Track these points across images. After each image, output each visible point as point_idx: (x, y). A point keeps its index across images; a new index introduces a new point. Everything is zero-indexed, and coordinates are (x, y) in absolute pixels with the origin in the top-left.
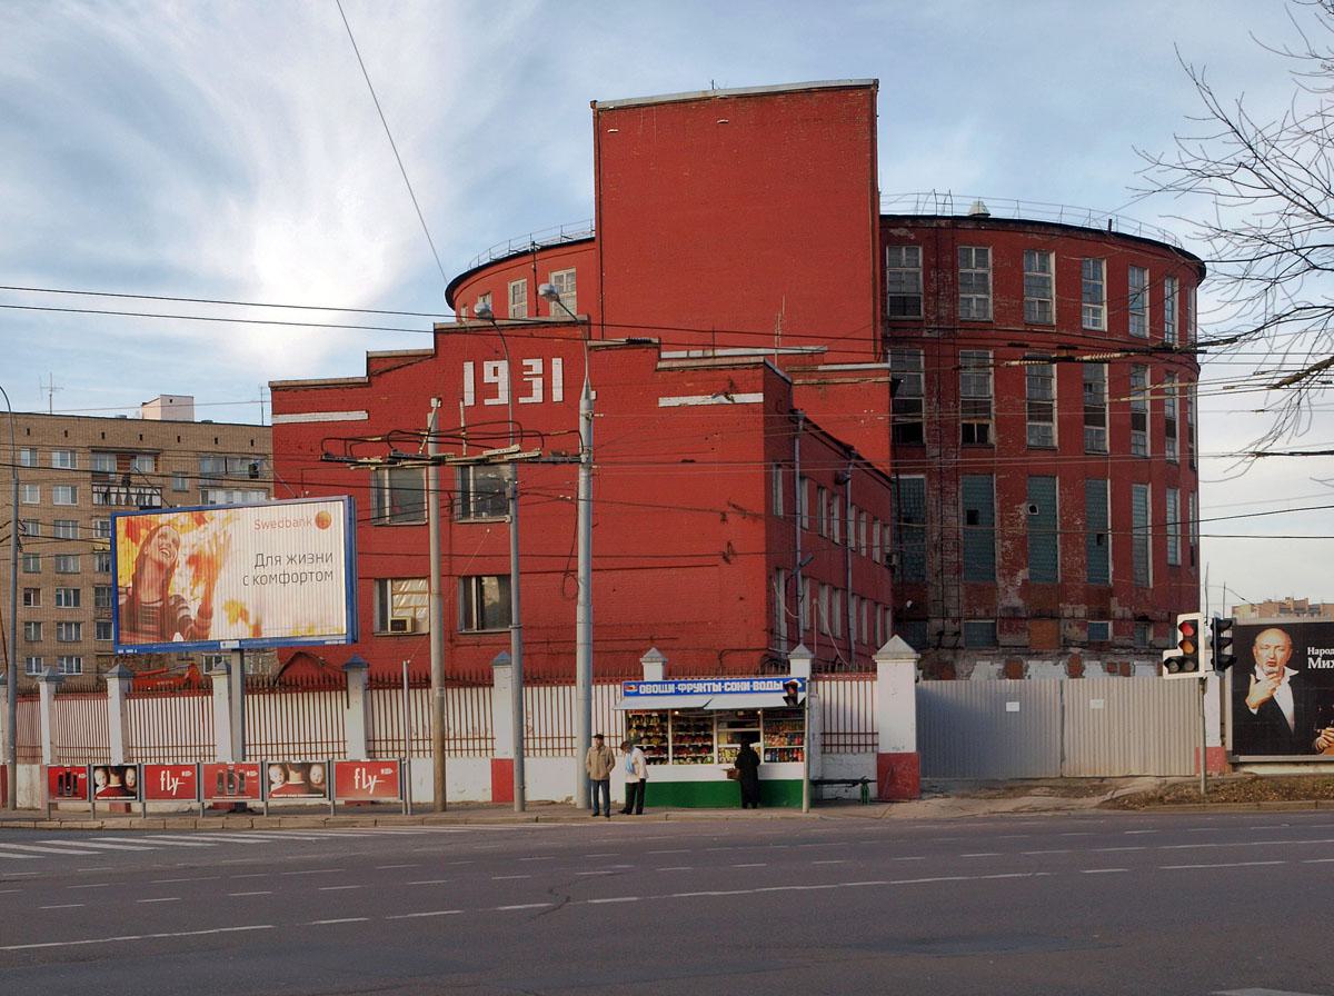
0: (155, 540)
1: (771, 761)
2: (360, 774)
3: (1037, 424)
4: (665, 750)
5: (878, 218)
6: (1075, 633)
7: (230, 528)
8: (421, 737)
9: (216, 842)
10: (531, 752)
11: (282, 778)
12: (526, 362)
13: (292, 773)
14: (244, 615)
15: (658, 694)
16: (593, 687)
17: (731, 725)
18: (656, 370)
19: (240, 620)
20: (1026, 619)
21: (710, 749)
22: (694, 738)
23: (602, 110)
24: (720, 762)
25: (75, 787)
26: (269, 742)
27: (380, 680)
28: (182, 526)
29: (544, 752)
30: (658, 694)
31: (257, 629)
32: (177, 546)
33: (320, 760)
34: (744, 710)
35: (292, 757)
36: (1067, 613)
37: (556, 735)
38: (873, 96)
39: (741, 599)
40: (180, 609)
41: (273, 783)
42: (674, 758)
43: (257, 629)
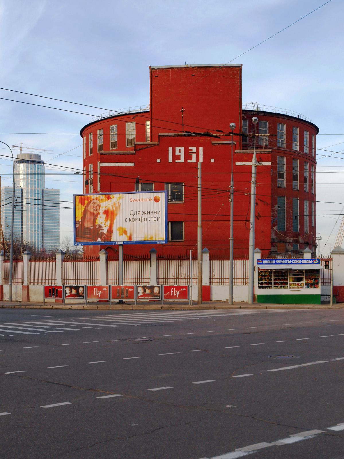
0: (91, 204)
1: (307, 288)
2: (173, 290)
3: (280, 179)
4: (271, 283)
5: (241, 111)
6: (290, 247)
7: (121, 201)
8: (175, 277)
9: (228, 315)
10: (214, 283)
11: (143, 291)
12: (190, 148)
13: (147, 290)
14: (125, 232)
15: (269, 264)
16: (234, 261)
17: (294, 275)
18: (235, 153)
19: (124, 234)
20: (277, 242)
21: (287, 283)
22: (280, 280)
23: (153, 69)
24: (290, 288)
25: (57, 294)
26: (69, 279)
27: (136, 257)
28: (101, 200)
29: (218, 283)
30: (269, 264)
31: (130, 238)
32: (100, 207)
33: (82, 285)
34: (299, 270)
35: (73, 284)
36: (288, 241)
37: (138, 278)
38: (241, 70)
39: (263, 232)
40: (100, 230)
41: (67, 293)
42: (274, 286)
43: (130, 238)
